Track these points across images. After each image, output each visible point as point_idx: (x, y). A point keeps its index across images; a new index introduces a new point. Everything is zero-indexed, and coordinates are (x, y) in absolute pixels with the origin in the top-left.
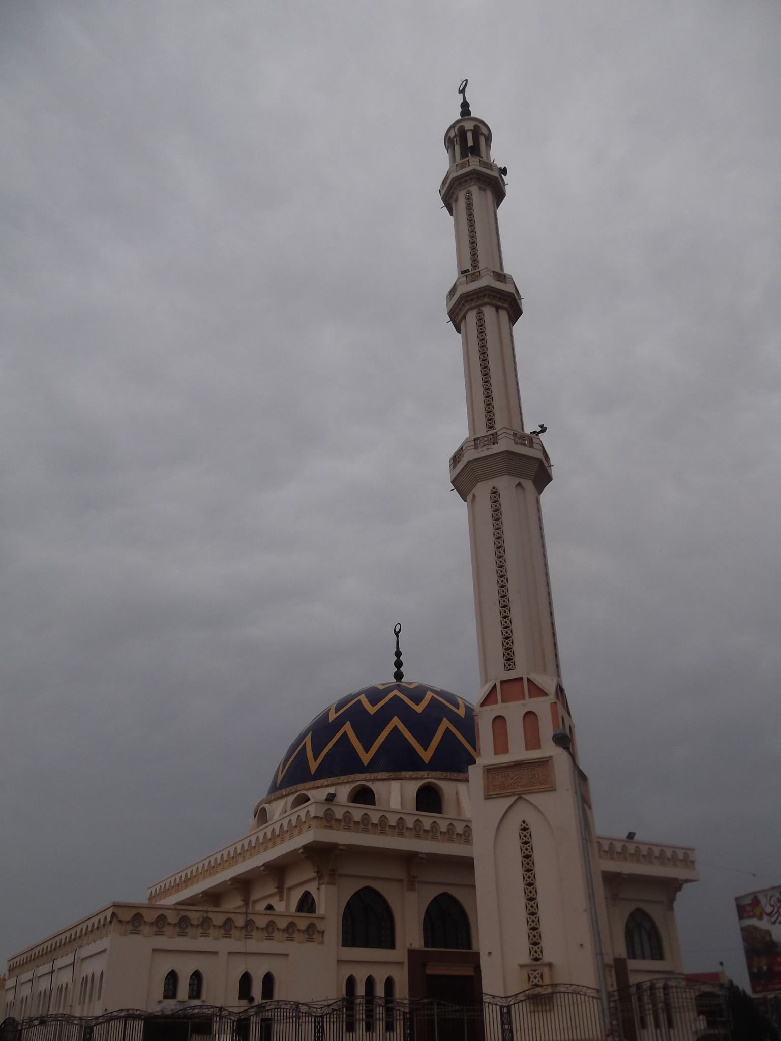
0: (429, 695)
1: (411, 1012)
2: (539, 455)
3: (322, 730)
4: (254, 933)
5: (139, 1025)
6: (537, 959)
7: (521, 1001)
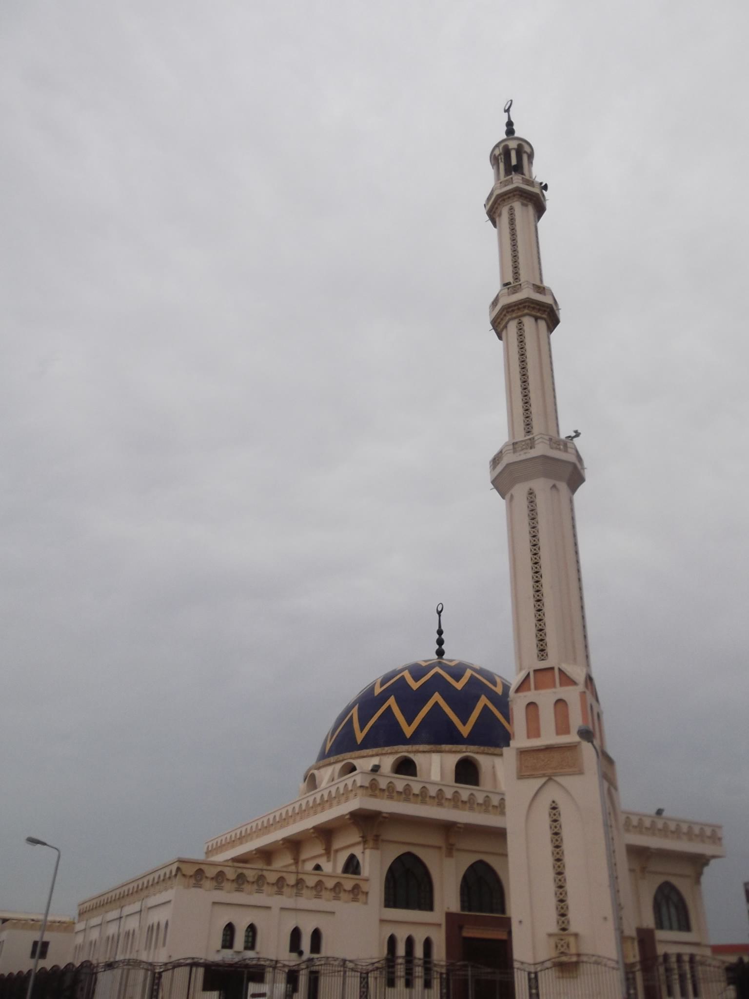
0: (468, 673)
1: (447, 974)
2: (572, 458)
3: (368, 703)
4: (304, 891)
5: (201, 971)
6: (564, 929)
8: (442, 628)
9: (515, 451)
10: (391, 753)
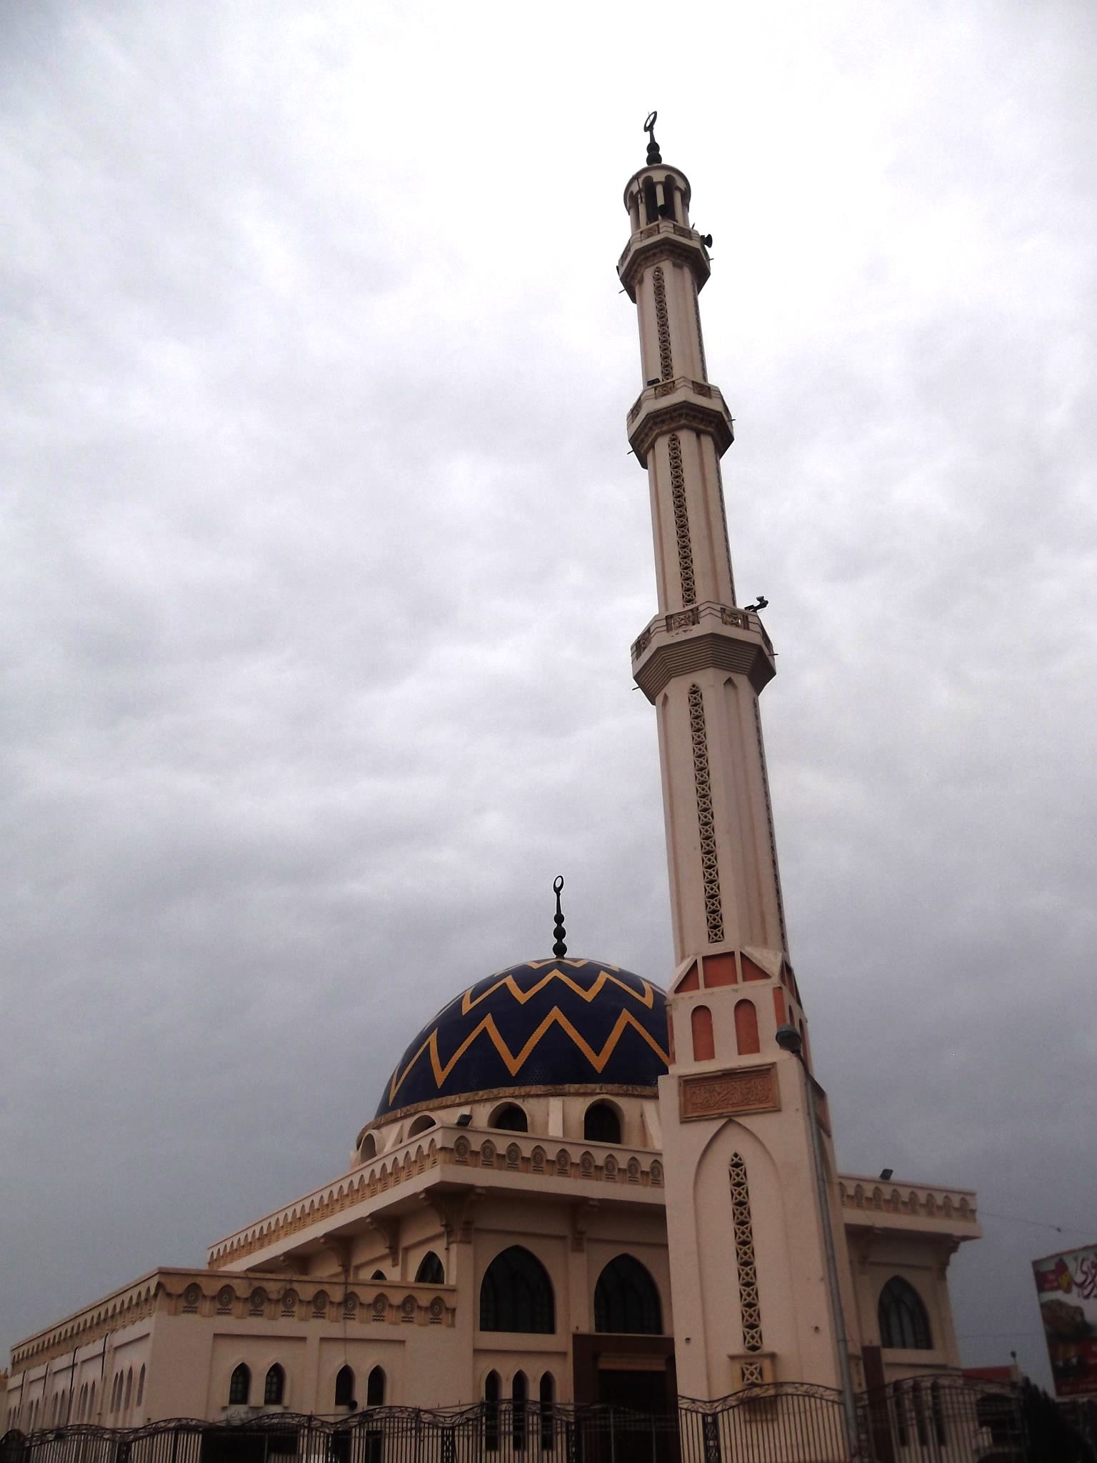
0: (603, 977)
1: (577, 1422)
2: (757, 640)
3: (452, 1025)
5: (196, 1441)
6: (754, 1348)
7: (732, 1407)
9: (669, 628)
10: (487, 1100)
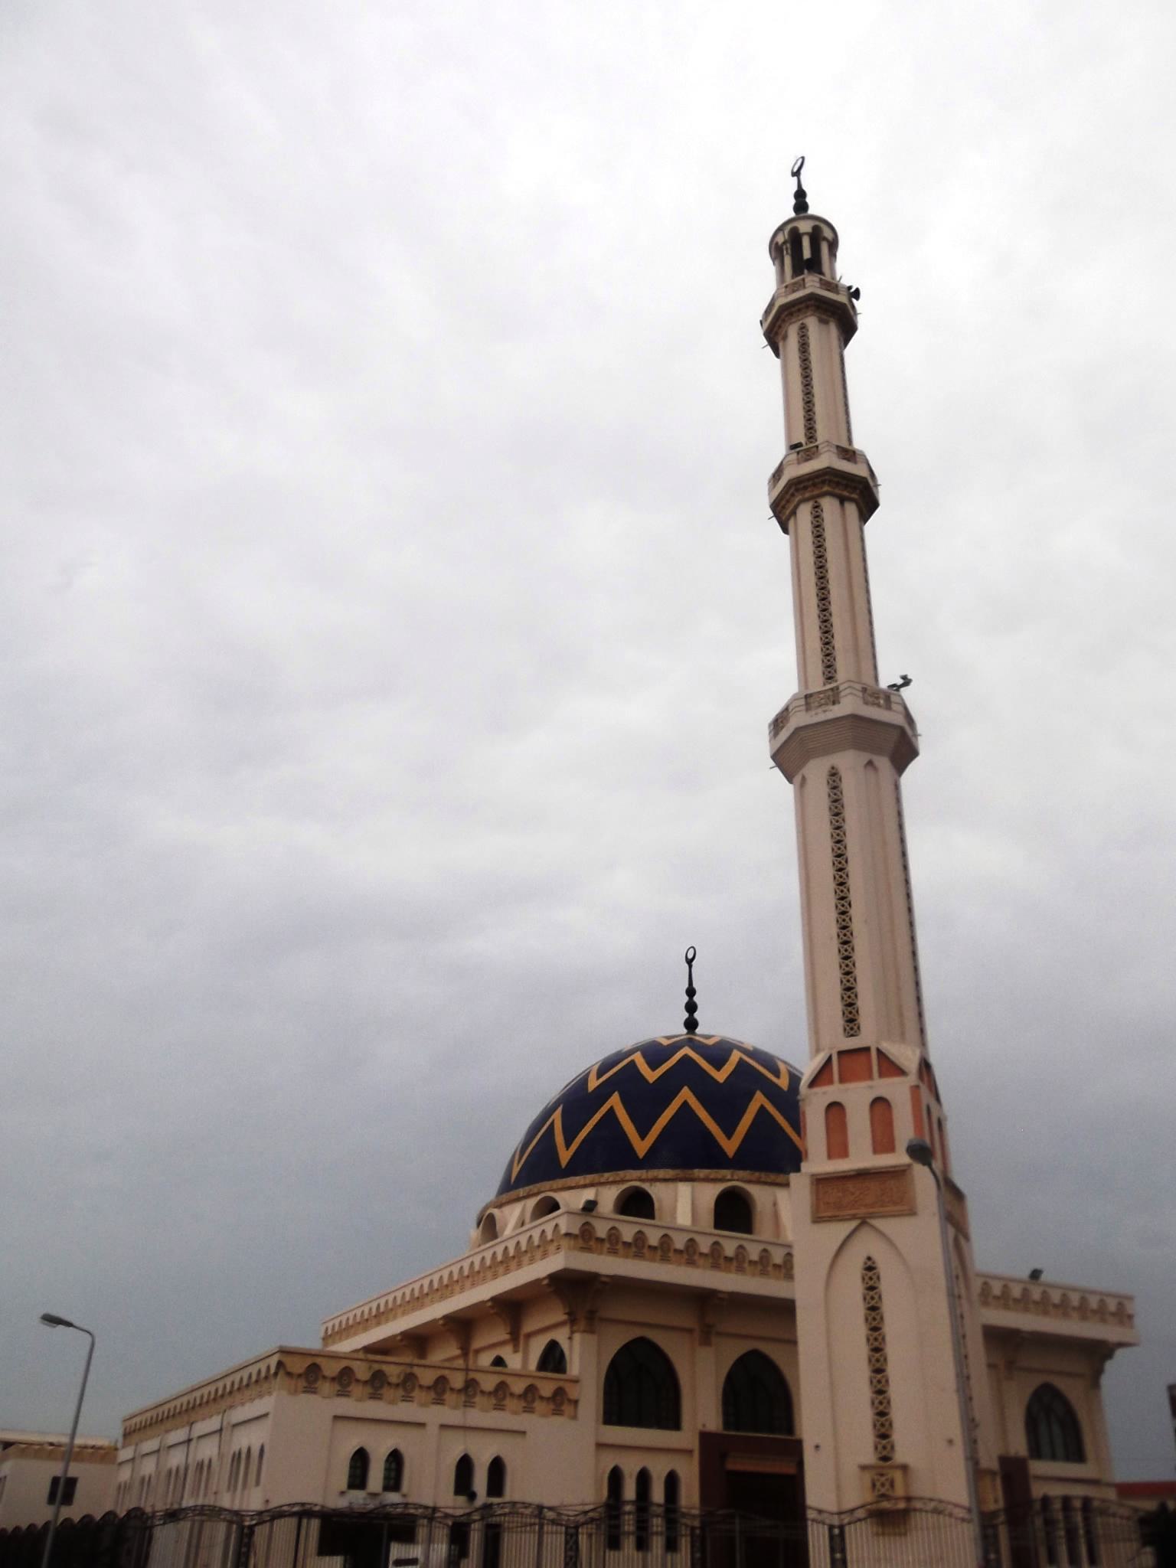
0: (736, 1056)
1: (702, 1528)
3: (577, 1102)
5: (315, 1523)
6: (885, 1459)
7: (860, 1520)
8: (695, 985)
9: (808, 707)
